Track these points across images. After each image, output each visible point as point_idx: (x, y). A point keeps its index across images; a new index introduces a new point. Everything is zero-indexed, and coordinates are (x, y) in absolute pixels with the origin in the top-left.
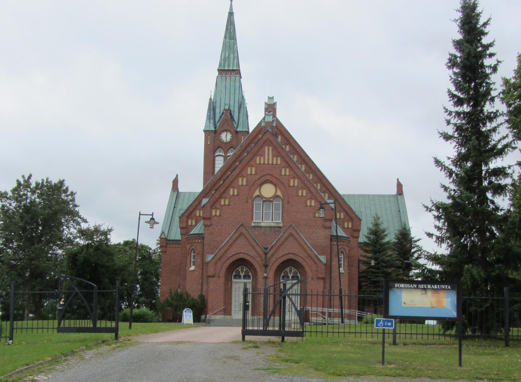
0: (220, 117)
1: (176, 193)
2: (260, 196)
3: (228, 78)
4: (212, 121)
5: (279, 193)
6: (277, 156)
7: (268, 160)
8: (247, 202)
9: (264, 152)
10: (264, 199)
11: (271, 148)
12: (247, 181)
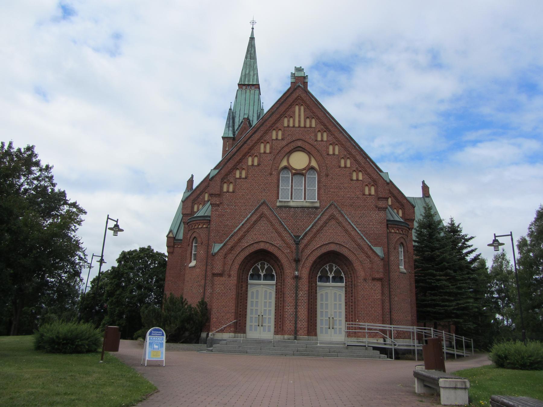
0: (239, 126)
4: (231, 129)
7: (299, 121)
9: (294, 112)
10: (294, 171)
11: (302, 108)
12: (271, 148)
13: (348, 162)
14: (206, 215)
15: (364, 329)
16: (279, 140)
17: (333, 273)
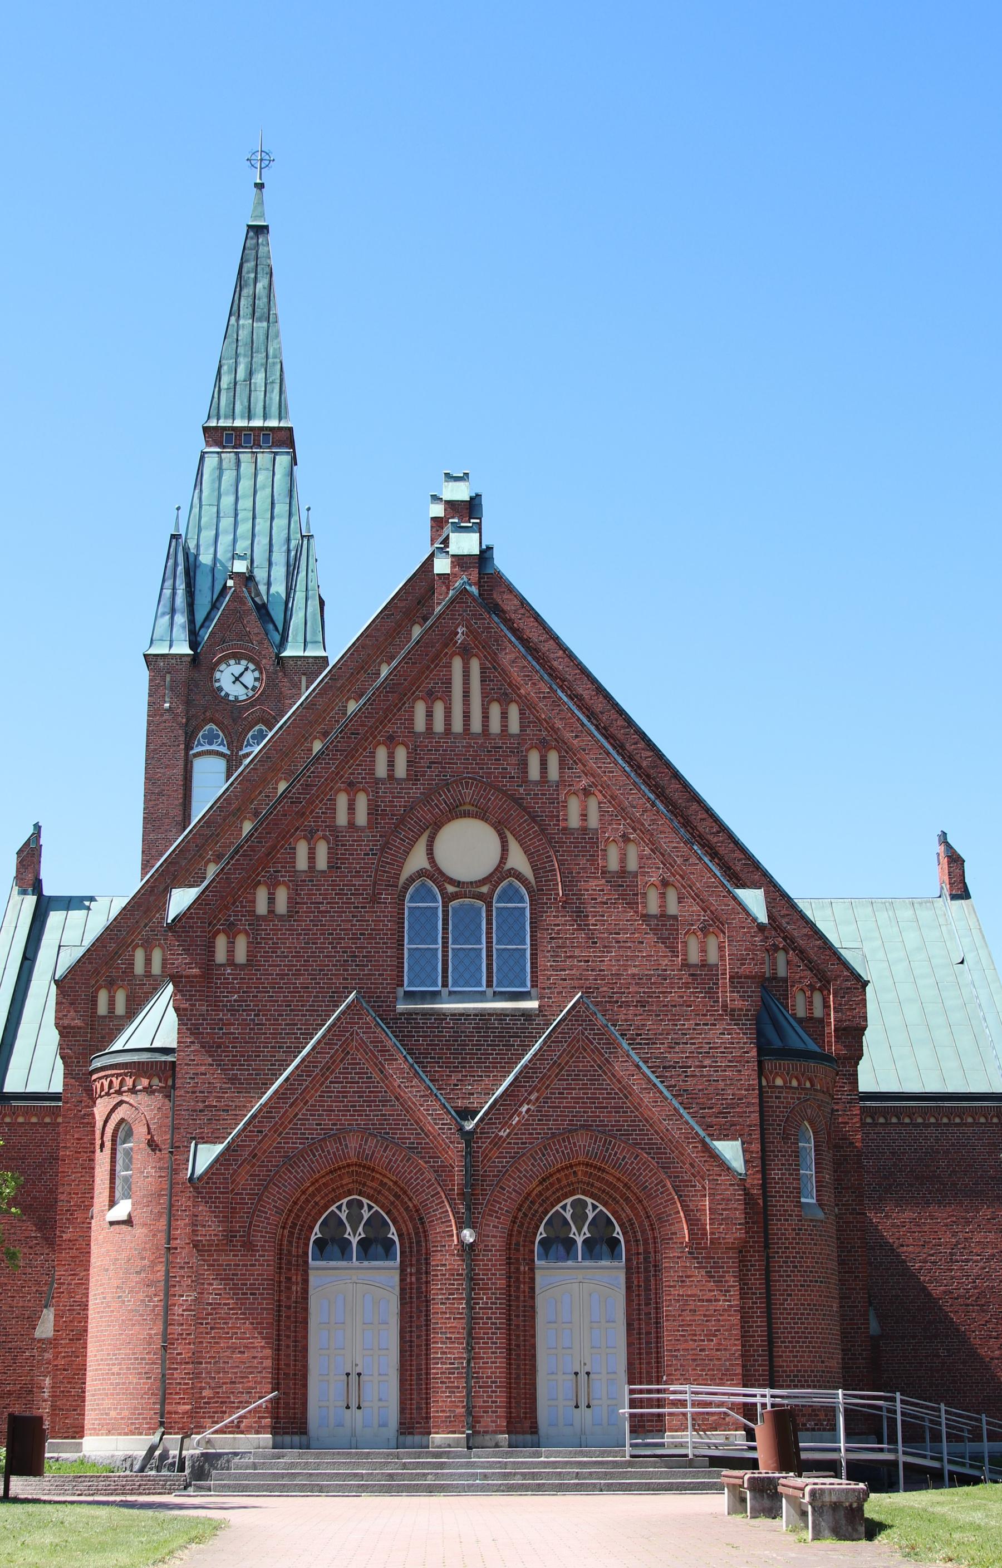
0: (214, 606)
1: (31, 900)
2: (435, 874)
3: (246, 458)
4: (181, 619)
5: (518, 860)
6: (504, 701)
7: (467, 716)
8: (374, 899)
9: (448, 683)
10: (451, 889)
11: (475, 665)
12: (373, 811)
13: (633, 853)
14: (157, 1044)
15: (683, 1403)
16: (399, 781)
17: (585, 1229)
